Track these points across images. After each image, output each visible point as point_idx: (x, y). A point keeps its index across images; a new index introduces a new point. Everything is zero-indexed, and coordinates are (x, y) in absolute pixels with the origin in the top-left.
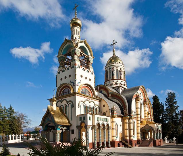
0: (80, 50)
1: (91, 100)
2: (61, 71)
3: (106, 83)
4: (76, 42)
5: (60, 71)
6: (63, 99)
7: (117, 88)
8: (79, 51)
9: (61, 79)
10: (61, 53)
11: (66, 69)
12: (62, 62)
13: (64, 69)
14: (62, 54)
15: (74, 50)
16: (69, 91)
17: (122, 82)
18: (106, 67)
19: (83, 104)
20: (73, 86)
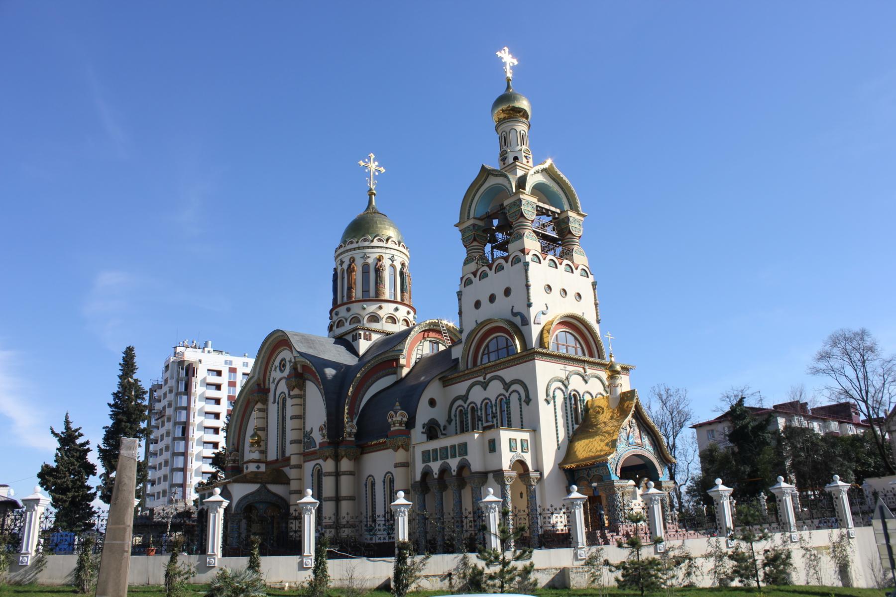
0: (535, 200)
1: (589, 371)
2: (475, 276)
3: (337, 314)
4: (520, 173)
5: (472, 276)
6: (488, 376)
7: (353, 336)
8: (531, 203)
9: (478, 305)
10: (469, 213)
11: (491, 269)
12: (475, 243)
13: (486, 269)
14: (472, 216)
15: (514, 202)
16: (509, 347)
17: (397, 309)
18: (342, 250)
19: (563, 388)
20: (523, 329)
